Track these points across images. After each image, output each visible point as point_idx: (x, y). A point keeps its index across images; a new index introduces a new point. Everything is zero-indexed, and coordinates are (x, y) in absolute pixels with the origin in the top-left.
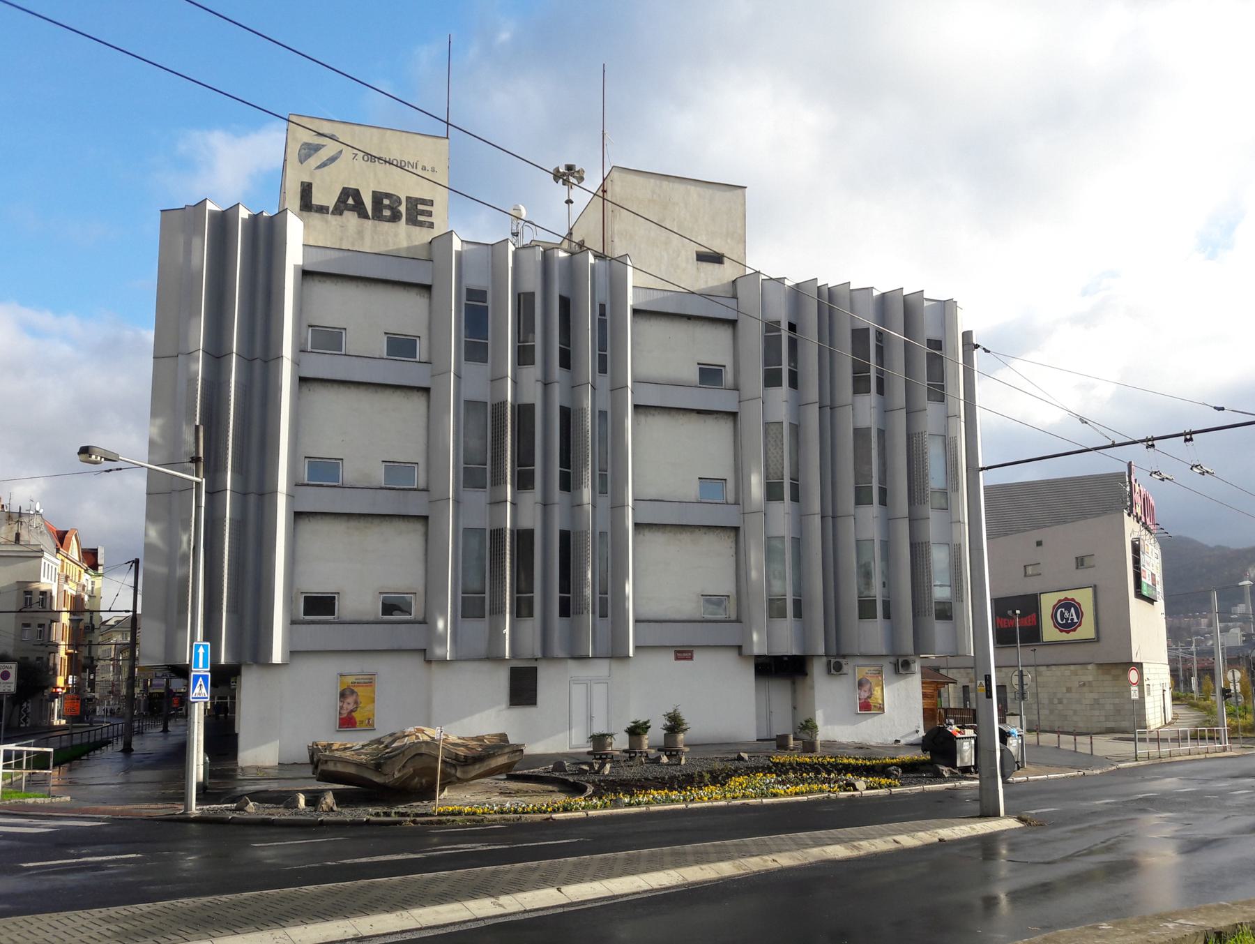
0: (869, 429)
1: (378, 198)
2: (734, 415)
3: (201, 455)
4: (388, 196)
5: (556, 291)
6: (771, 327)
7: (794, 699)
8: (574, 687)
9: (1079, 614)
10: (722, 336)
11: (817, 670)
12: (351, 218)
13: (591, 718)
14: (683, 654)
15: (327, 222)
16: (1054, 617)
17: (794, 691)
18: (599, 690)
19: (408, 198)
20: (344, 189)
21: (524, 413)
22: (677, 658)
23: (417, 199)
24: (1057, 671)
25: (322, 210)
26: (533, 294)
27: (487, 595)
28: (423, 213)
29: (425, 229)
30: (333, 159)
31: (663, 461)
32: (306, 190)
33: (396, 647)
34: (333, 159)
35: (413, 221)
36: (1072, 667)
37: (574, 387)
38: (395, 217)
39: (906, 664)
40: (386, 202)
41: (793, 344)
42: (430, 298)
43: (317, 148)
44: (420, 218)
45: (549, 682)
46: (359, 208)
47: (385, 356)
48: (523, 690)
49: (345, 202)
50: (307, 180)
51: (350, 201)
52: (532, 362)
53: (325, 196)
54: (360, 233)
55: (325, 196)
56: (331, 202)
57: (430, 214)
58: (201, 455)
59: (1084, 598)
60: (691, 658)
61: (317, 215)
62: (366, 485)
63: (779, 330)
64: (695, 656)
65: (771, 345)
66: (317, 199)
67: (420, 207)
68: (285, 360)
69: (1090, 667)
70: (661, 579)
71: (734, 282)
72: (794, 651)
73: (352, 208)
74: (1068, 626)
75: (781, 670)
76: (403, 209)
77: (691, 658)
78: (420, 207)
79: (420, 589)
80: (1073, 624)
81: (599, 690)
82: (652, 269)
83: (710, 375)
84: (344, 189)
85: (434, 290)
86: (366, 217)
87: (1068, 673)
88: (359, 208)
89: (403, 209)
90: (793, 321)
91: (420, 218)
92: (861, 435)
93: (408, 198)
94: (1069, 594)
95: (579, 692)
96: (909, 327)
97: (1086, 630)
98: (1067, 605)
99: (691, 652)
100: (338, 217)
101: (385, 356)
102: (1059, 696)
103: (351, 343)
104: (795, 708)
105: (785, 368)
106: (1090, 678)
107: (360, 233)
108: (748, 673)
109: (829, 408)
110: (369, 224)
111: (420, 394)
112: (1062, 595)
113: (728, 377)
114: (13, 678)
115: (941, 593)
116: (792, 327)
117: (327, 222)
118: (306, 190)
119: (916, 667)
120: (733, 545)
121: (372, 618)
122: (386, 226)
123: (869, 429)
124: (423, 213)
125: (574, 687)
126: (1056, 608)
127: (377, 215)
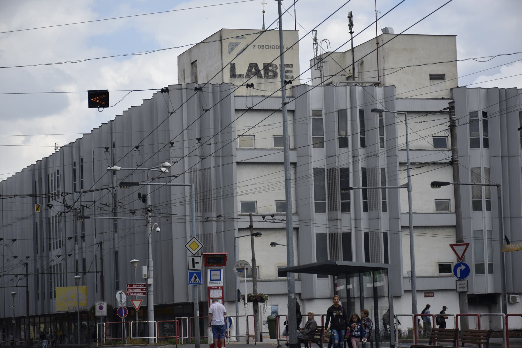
0: (326, 234)
3: (249, 213)
4: (270, 64)
6: (473, 114)
21: (344, 172)
22: (425, 296)
28: (287, 72)
32: (233, 67)
37: (371, 156)
40: (270, 68)
41: (485, 123)
42: (294, 115)
43: (237, 45)
46: (257, 73)
49: (251, 71)
51: (254, 70)
53: (242, 69)
55: (242, 69)
58: (249, 213)
61: (239, 79)
63: (477, 116)
64: (435, 295)
65: (473, 123)
66: (237, 72)
67: (287, 69)
68: (362, 221)
71: (451, 89)
76: (278, 71)
77: (433, 296)
82: (409, 85)
85: (297, 113)
86: (261, 77)
88: (257, 73)
89: (278, 71)
99: (433, 293)
101: (273, 147)
104: (490, 322)
105: (481, 137)
110: (263, 80)
111: (452, 292)
114: (105, 309)
116: (485, 114)
121: (274, 279)
122: (271, 80)
123: (326, 234)
124: (287, 72)
127: (266, 76)
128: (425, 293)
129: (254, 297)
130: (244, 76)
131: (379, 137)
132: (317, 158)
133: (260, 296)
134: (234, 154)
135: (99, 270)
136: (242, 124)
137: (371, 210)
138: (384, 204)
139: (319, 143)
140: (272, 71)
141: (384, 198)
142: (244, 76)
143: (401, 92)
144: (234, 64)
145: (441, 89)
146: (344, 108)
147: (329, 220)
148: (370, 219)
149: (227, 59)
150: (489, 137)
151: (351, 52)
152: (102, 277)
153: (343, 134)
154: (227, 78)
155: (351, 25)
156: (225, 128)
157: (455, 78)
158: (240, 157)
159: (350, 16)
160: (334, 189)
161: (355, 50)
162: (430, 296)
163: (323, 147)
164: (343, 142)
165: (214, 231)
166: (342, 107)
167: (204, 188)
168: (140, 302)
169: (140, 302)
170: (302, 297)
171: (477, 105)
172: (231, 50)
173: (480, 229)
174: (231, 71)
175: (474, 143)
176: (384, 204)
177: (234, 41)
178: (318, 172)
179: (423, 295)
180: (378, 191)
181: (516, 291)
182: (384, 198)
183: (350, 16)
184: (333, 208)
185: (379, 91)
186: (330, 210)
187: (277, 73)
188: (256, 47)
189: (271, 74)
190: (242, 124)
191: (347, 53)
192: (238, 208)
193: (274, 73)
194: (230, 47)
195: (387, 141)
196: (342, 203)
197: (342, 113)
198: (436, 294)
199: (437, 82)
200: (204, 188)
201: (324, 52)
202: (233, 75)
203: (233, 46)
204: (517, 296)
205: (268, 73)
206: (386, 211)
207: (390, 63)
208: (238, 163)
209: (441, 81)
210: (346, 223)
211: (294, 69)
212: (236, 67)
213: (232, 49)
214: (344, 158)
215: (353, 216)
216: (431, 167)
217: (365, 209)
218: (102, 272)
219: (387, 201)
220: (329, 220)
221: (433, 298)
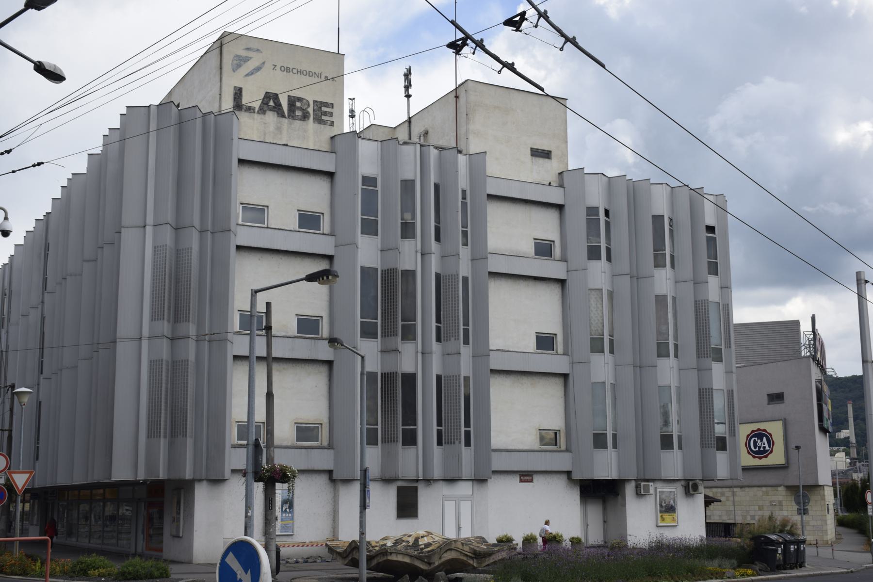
1: (292, 101)
2: (562, 282)
4: (300, 99)
5: (433, 179)
6: (592, 211)
7: (362, 533)
8: (446, 503)
9: (771, 443)
10: (321, 186)
11: (629, 490)
12: (271, 117)
13: (460, 528)
14: (526, 476)
15: (254, 119)
16: (748, 444)
17: (605, 509)
18: (465, 506)
19: (315, 102)
20: (267, 93)
22: (521, 481)
23: (322, 103)
24: (751, 492)
25: (250, 109)
26: (413, 181)
27: (379, 427)
28: (325, 113)
29: (328, 127)
30: (258, 69)
31: (516, 319)
32: (238, 93)
33: (310, 468)
34: (258, 69)
35: (319, 120)
36: (764, 489)
38: (305, 117)
39: (695, 488)
40: (298, 104)
42: (332, 182)
43: (247, 59)
44: (324, 118)
45: (426, 498)
47: (297, 229)
48: (407, 506)
49: (267, 104)
50: (239, 85)
51: (271, 103)
52: (414, 237)
53: (252, 97)
54: (279, 129)
55: (252, 97)
56: (257, 105)
57: (331, 114)
59: (775, 429)
60: (532, 481)
61: (247, 114)
62: (283, 334)
63: (598, 215)
65: (592, 225)
66: (245, 100)
67: (324, 109)
68: (434, 355)
69: (780, 489)
70: (519, 416)
71: (560, 174)
72: (613, 475)
73: (272, 109)
74: (761, 453)
75: (600, 493)
77: (532, 481)
78: (324, 109)
79: (325, 420)
80: (765, 451)
81: (465, 506)
83: (543, 249)
84: (267, 93)
85: (337, 178)
86: (283, 116)
87: (760, 493)
90: (607, 208)
91: (324, 118)
92: (661, 300)
93: (315, 102)
94: (762, 426)
95: (450, 506)
96: (695, 212)
97: (777, 457)
98: (760, 434)
99: (532, 476)
100: (261, 116)
102: (752, 513)
103: (274, 219)
104: (605, 522)
106: (781, 498)
107: (279, 129)
108: (574, 496)
109: (637, 277)
110: (285, 121)
111: (558, 476)
112: (755, 426)
113: (557, 251)
115: (720, 430)
116: (607, 213)
117: (254, 119)
118: (238, 93)
119: (701, 488)
120: (563, 389)
121: (289, 444)
122: (298, 123)
124: (325, 113)
125: (446, 503)
126: (749, 437)
127: (292, 114)
128: (521, 476)
129: (267, 471)
130: (256, 110)
131: (461, 229)
132: (367, 252)
133: (281, 470)
134: (233, 228)
135: (7, 427)
136: (250, 188)
137: (448, 339)
138: (466, 332)
139: (370, 228)
140: (301, 109)
141: (466, 323)
142: (256, 110)
143: (493, 168)
144: (240, 90)
145: (547, 170)
146: (412, 178)
147: (382, 352)
148: (446, 354)
149: (232, 81)
150: (612, 247)
151: (407, 124)
152: (10, 438)
153: (408, 217)
154: (228, 104)
155: (407, 87)
156: (217, 186)
157: (564, 156)
158: (246, 236)
159: (407, 75)
160: (389, 301)
161: (412, 120)
162: (527, 481)
163: (377, 235)
164: (407, 230)
165: (192, 357)
166: (409, 176)
167: (177, 281)
168: (26, 476)
169: (26, 476)
170: (335, 477)
171: (596, 198)
172: (237, 67)
173: (601, 381)
174: (235, 99)
175: (594, 253)
176: (466, 332)
177: (244, 53)
178: (367, 273)
179: (517, 478)
180: (458, 312)
181: (647, 477)
182: (466, 323)
183: (407, 75)
184: (388, 332)
185: (462, 159)
186: (385, 335)
187: (308, 112)
188: (278, 68)
189: (298, 113)
190: (250, 188)
191: (398, 129)
192: (235, 323)
193: (303, 113)
194: (235, 62)
195: (473, 234)
196: (403, 326)
197: (408, 186)
198: (536, 478)
199: (541, 161)
200: (177, 281)
201: (367, 125)
202: (238, 105)
203: (240, 61)
204: (651, 484)
205: (294, 112)
206: (468, 344)
207: (478, 123)
208: (239, 248)
209: (547, 160)
210: (408, 360)
211: (335, 111)
212: (244, 93)
213: (239, 66)
214: (408, 256)
215: (420, 348)
216: (531, 283)
217: (439, 339)
218: (10, 431)
219: (470, 328)
220: (382, 352)
221: (531, 484)
